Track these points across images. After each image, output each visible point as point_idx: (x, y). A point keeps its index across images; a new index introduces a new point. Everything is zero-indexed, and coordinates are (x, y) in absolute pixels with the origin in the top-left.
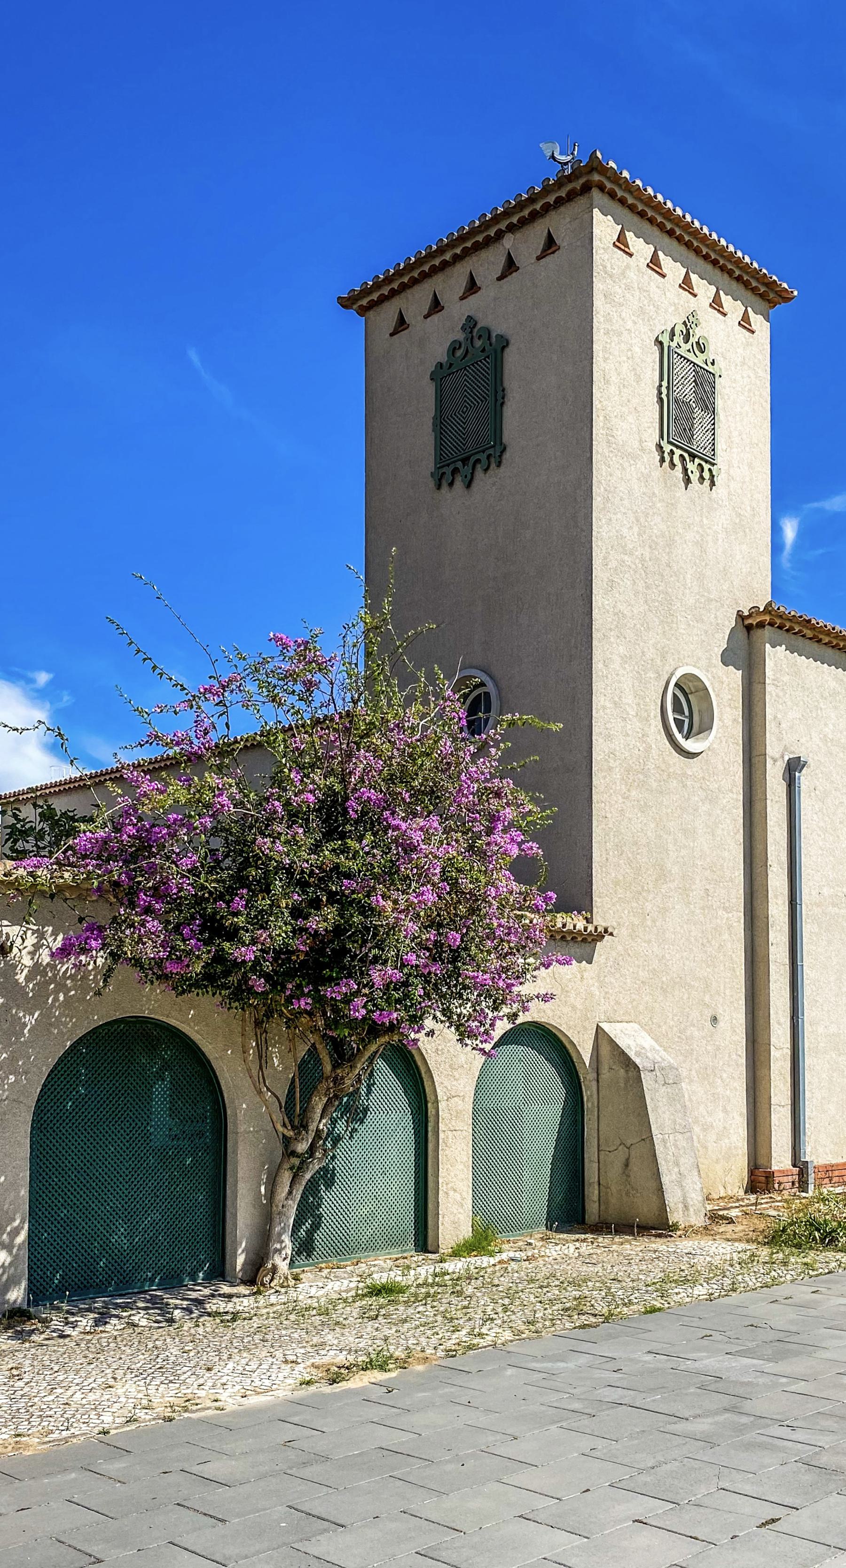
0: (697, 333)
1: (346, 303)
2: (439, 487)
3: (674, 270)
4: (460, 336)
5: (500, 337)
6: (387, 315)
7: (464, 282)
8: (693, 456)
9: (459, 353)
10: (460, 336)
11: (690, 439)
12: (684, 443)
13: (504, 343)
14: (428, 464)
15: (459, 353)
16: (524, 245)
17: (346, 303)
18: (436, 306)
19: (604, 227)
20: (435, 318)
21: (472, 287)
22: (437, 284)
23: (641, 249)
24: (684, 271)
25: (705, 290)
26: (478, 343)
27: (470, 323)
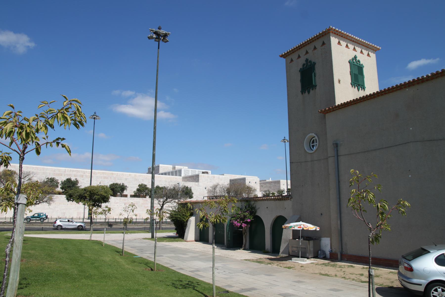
0: (358, 59)
1: (282, 56)
2: (2, 212)
3: (351, 46)
4: (305, 62)
5: (314, 62)
6: (289, 58)
7: (313, 48)
8: (359, 85)
9: (305, 66)
10: (305, 62)
11: (358, 82)
12: (356, 83)
13: (315, 64)
14: (300, 89)
15: (305, 66)
16: (318, 44)
17: (282, 56)
18: (299, 57)
19: (334, 40)
20: (324, 46)
21: (307, 53)
22: (307, 48)
23: (344, 43)
24: (353, 46)
25: (358, 49)
26: (309, 64)
27: (307, 60)
